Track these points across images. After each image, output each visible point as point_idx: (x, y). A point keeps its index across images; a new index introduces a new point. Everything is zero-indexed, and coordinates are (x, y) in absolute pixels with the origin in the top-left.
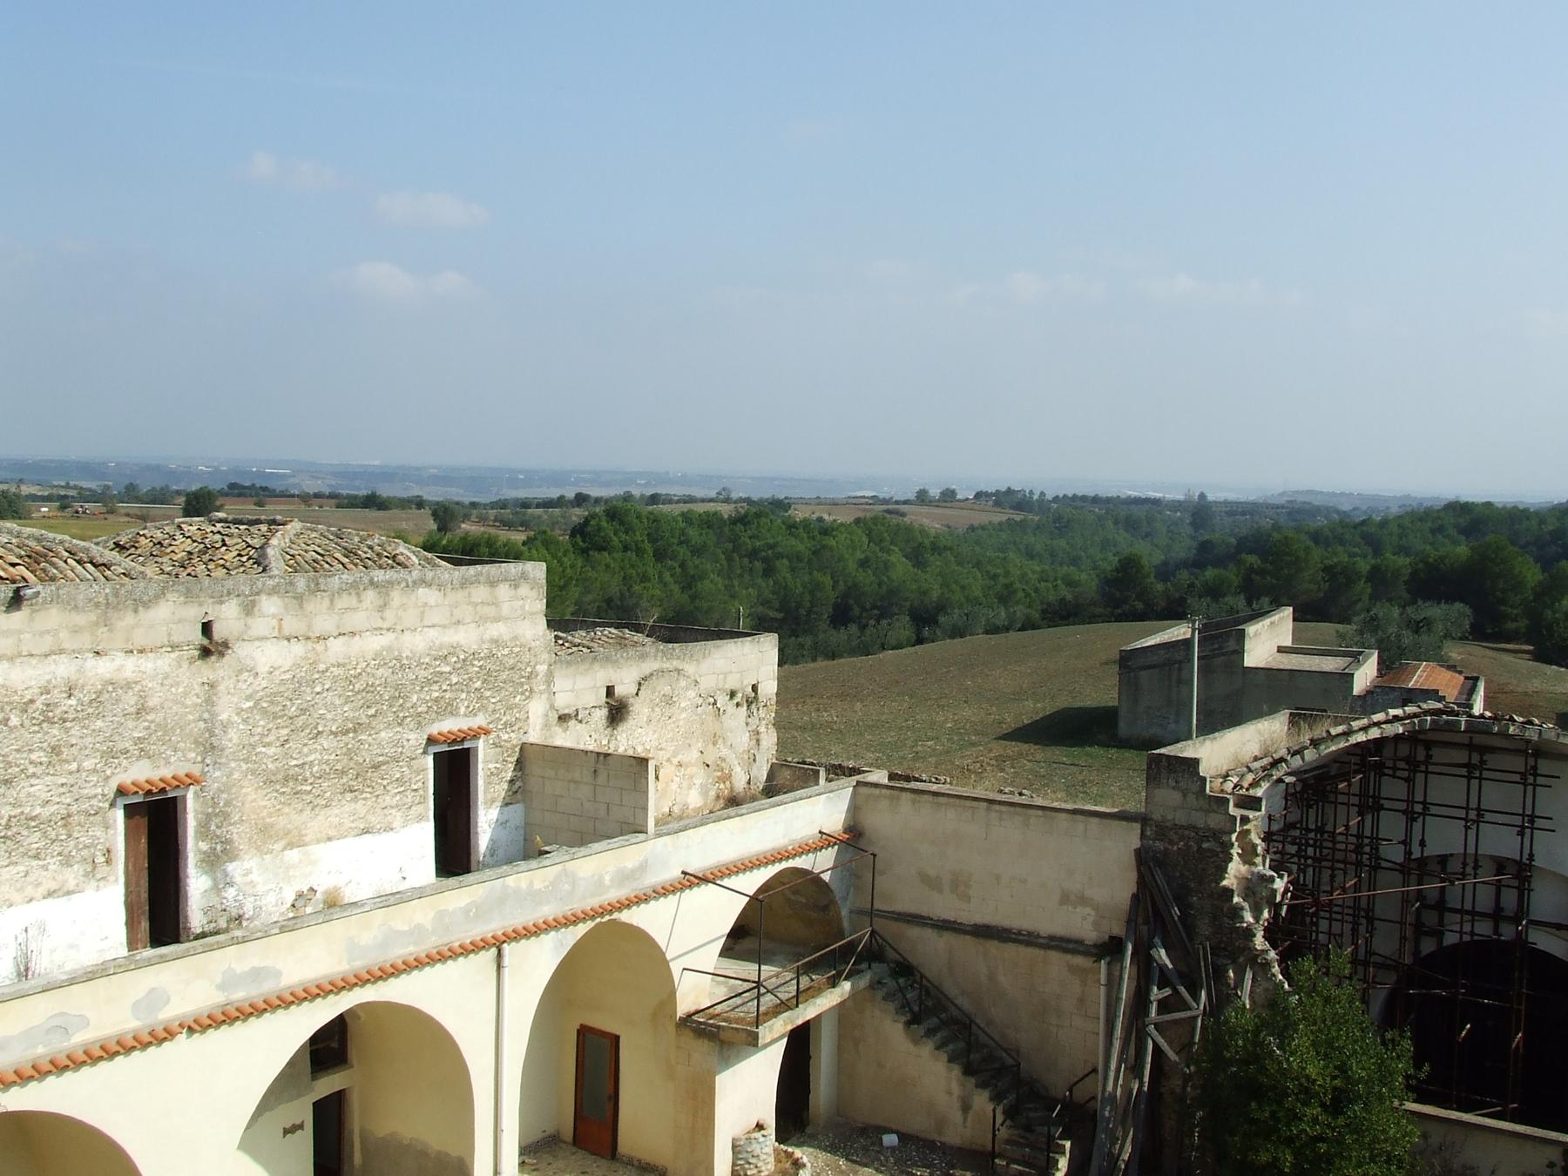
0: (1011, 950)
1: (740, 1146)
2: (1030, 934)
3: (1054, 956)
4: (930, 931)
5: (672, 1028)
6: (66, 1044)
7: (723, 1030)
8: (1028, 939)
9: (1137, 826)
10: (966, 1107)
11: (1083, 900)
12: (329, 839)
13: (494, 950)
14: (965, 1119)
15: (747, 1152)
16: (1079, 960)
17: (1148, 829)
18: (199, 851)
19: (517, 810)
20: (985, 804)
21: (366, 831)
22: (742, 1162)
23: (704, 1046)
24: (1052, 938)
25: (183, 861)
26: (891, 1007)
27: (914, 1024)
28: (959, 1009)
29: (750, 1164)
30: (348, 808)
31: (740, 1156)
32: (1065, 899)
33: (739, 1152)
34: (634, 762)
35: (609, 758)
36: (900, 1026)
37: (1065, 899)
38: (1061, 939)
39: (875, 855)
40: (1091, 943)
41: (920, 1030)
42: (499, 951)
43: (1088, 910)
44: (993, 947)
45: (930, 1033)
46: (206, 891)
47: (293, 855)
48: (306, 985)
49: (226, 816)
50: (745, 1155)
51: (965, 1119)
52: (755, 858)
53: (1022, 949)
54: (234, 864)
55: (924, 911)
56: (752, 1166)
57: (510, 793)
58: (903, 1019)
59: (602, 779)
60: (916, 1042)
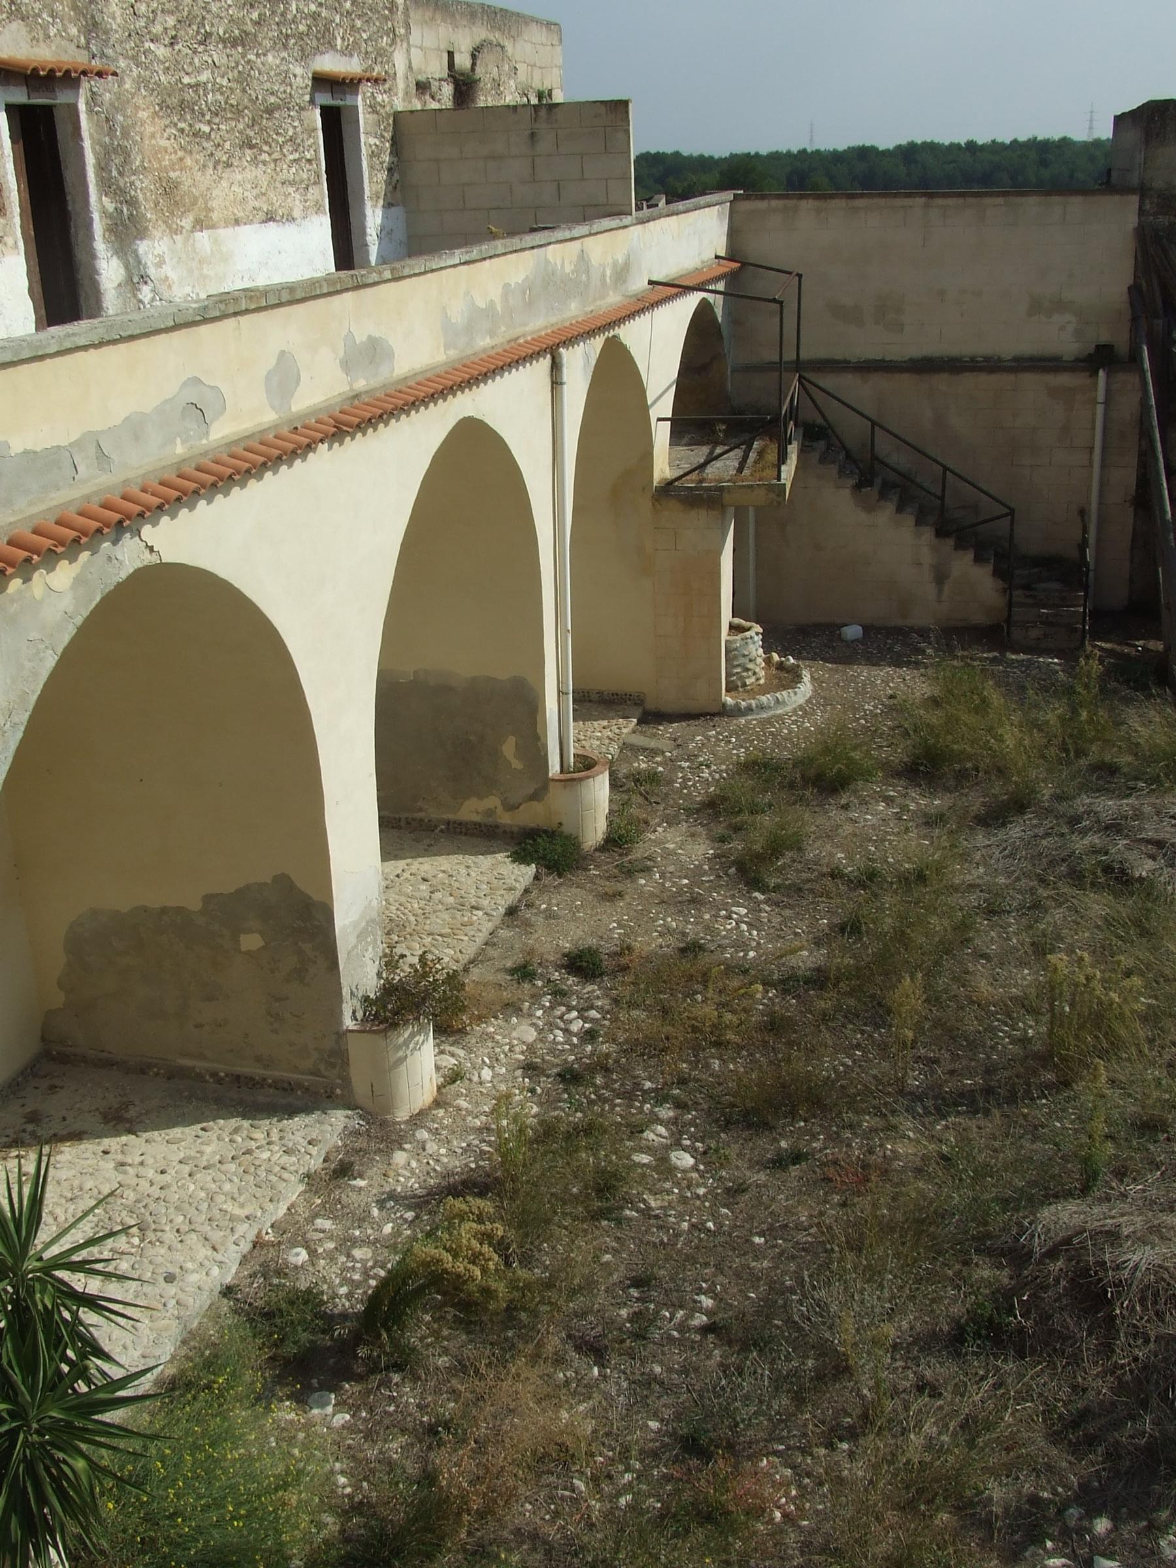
0: (969, 382)
1: (736, 649)
2: (987, 359)
3: (1030, 380)
4: (850, 376)
5: (646, 504)
6: (204, 441)
7: (729, 492)
8: (990, 365)
9: (1134, 199)
10: (940, 577)
11: (1060, 305)
12: (237, 222)
13: (545, 363)
14: (940, 591)
15: (744, 656)
16: (1064, 379)
17: (1147, 201)
18: (104, 212)
19: (397, 211)
20: (923, 199)
21: (270, 218)
22: (739, 670)
23: (701, 517)
24: (1016, 359)
25: (81, 233)
26: (833, 470)
27: (865, 487)
28: (894, 470)
29: (748, 670)
30: (251, 173)
31: (736, 663)
32: (1036, 307)
33: (736, 657)
34: (603, 109)
35: (556, 110)
36: (846, 493)
37: (1036, 307)
38: (1031, 359)
39: (800, 276)
40: (1072, 358)
41: (872, 492)
42: (553, 358)
43: (1069, 317)
44: (942, 382)
45: (883, 496)
46: (120, 285)
47: (203, 238)
48: (36, 522)
49: (126, 154)
50: (742, 660)
51: (940, 591)
52: (338, 409)
53: (983, 378)
54: (145, 242)
55: (838, 354)
56: (750, 673)
57: (390, 188)
58: (852, 482)
59: (545, 144)
60: (869, 508)
